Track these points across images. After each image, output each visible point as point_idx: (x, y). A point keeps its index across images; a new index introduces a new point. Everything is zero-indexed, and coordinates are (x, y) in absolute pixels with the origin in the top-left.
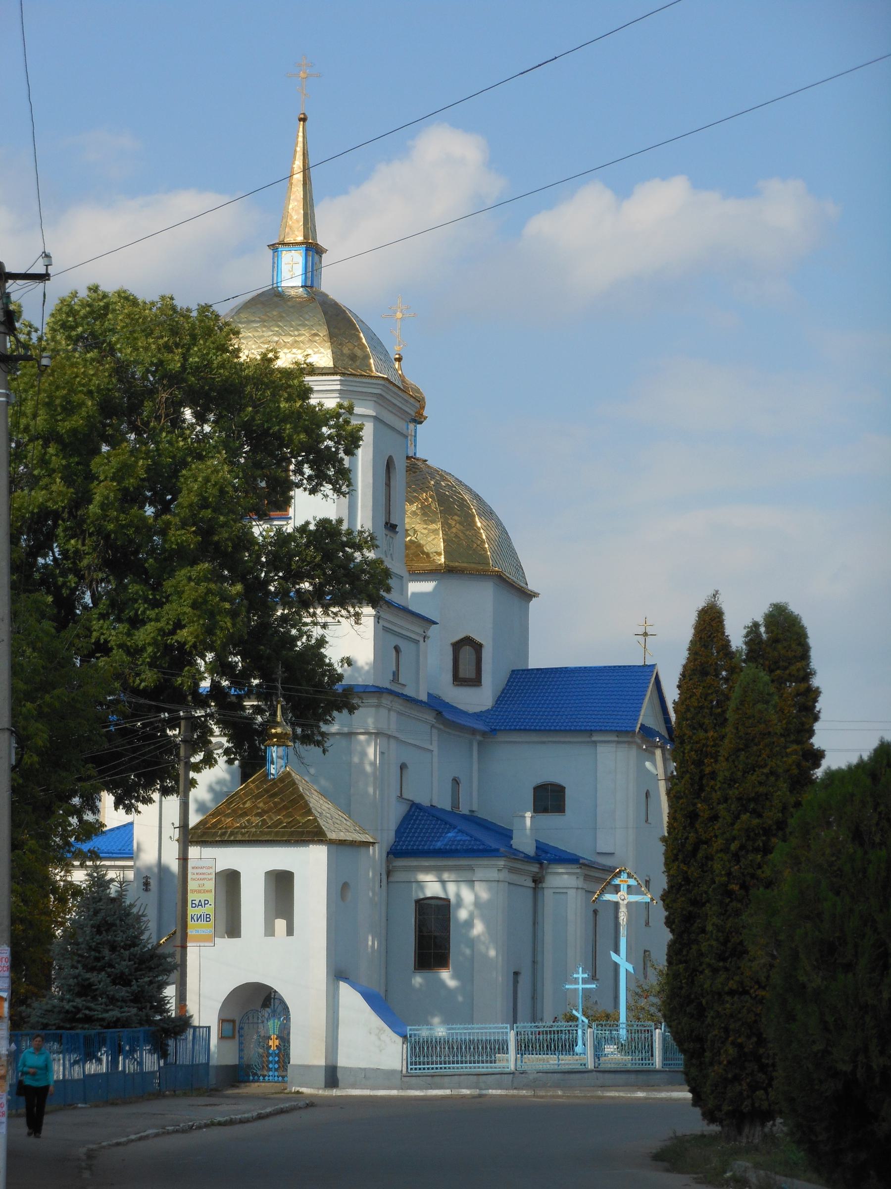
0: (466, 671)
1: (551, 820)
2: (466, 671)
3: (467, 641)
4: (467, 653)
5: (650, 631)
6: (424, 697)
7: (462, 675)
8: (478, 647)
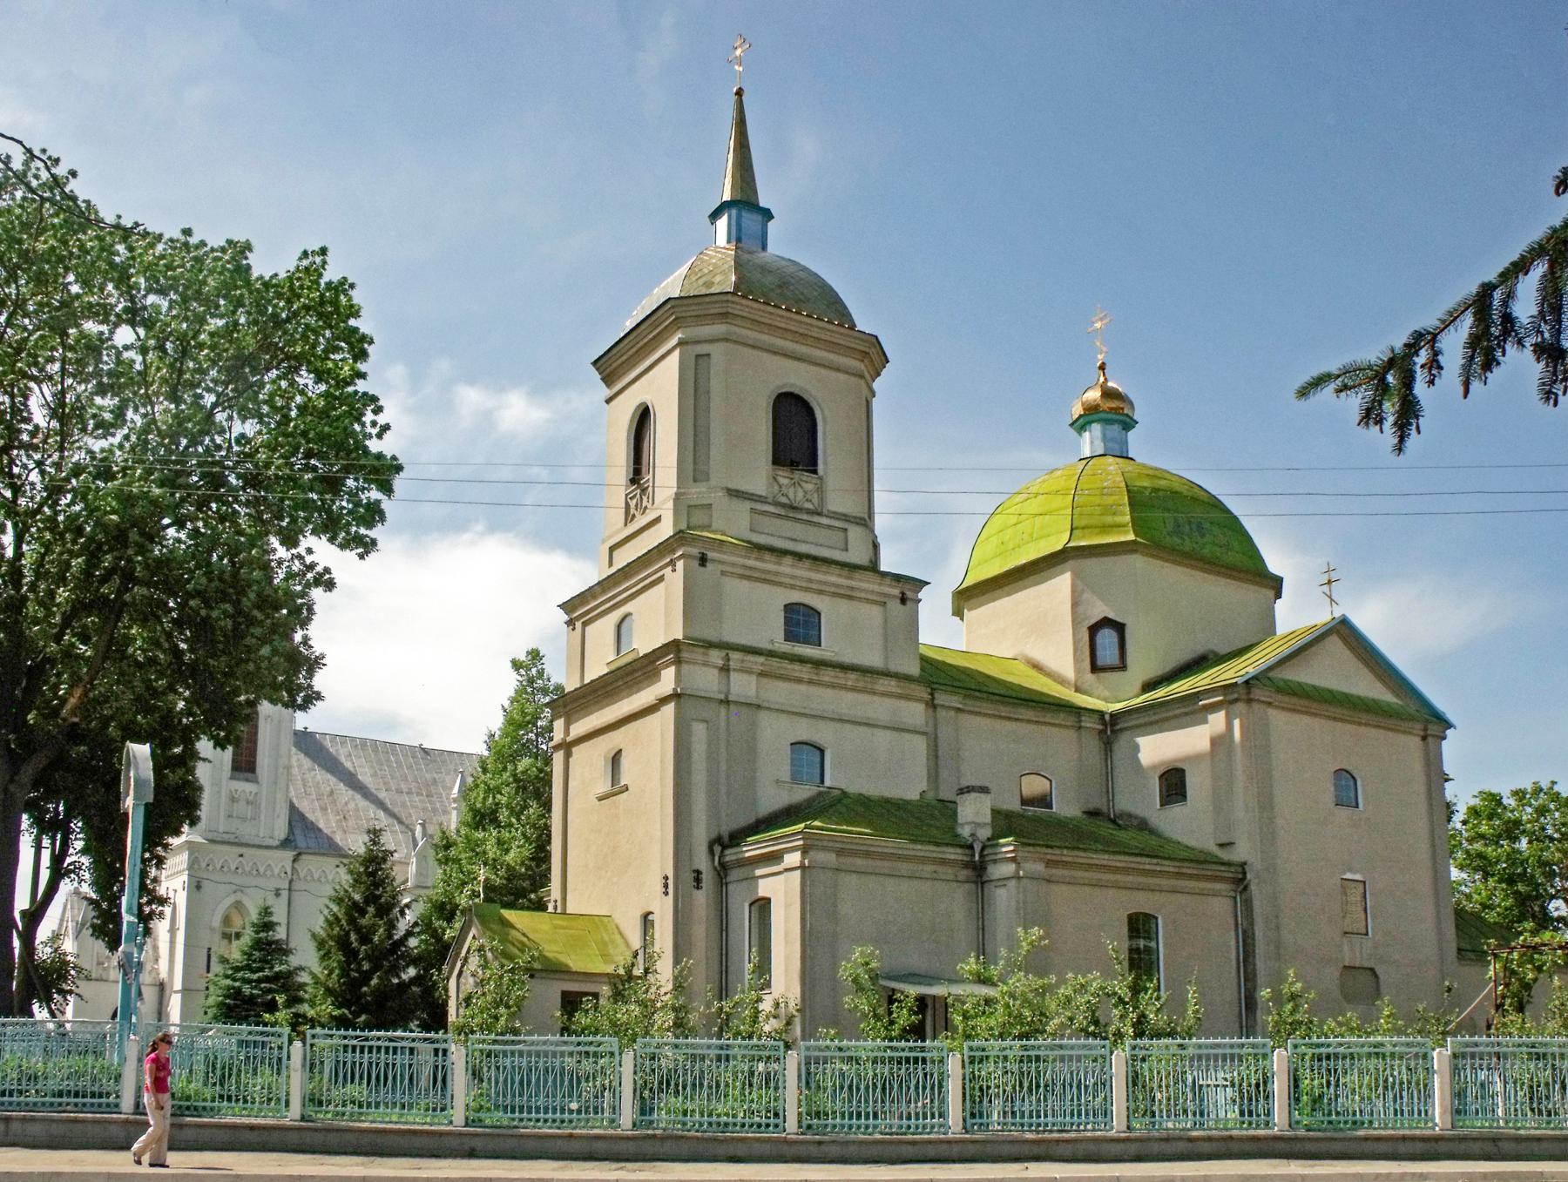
0: (1108, 654)
1: (1176, 810)
2: (1108, 654)
3: (1106, 622)
4: (1107, 638)
5: (1334, 576)
6: (914, 669)
7: (1100, 663)
8: (1120, 628)
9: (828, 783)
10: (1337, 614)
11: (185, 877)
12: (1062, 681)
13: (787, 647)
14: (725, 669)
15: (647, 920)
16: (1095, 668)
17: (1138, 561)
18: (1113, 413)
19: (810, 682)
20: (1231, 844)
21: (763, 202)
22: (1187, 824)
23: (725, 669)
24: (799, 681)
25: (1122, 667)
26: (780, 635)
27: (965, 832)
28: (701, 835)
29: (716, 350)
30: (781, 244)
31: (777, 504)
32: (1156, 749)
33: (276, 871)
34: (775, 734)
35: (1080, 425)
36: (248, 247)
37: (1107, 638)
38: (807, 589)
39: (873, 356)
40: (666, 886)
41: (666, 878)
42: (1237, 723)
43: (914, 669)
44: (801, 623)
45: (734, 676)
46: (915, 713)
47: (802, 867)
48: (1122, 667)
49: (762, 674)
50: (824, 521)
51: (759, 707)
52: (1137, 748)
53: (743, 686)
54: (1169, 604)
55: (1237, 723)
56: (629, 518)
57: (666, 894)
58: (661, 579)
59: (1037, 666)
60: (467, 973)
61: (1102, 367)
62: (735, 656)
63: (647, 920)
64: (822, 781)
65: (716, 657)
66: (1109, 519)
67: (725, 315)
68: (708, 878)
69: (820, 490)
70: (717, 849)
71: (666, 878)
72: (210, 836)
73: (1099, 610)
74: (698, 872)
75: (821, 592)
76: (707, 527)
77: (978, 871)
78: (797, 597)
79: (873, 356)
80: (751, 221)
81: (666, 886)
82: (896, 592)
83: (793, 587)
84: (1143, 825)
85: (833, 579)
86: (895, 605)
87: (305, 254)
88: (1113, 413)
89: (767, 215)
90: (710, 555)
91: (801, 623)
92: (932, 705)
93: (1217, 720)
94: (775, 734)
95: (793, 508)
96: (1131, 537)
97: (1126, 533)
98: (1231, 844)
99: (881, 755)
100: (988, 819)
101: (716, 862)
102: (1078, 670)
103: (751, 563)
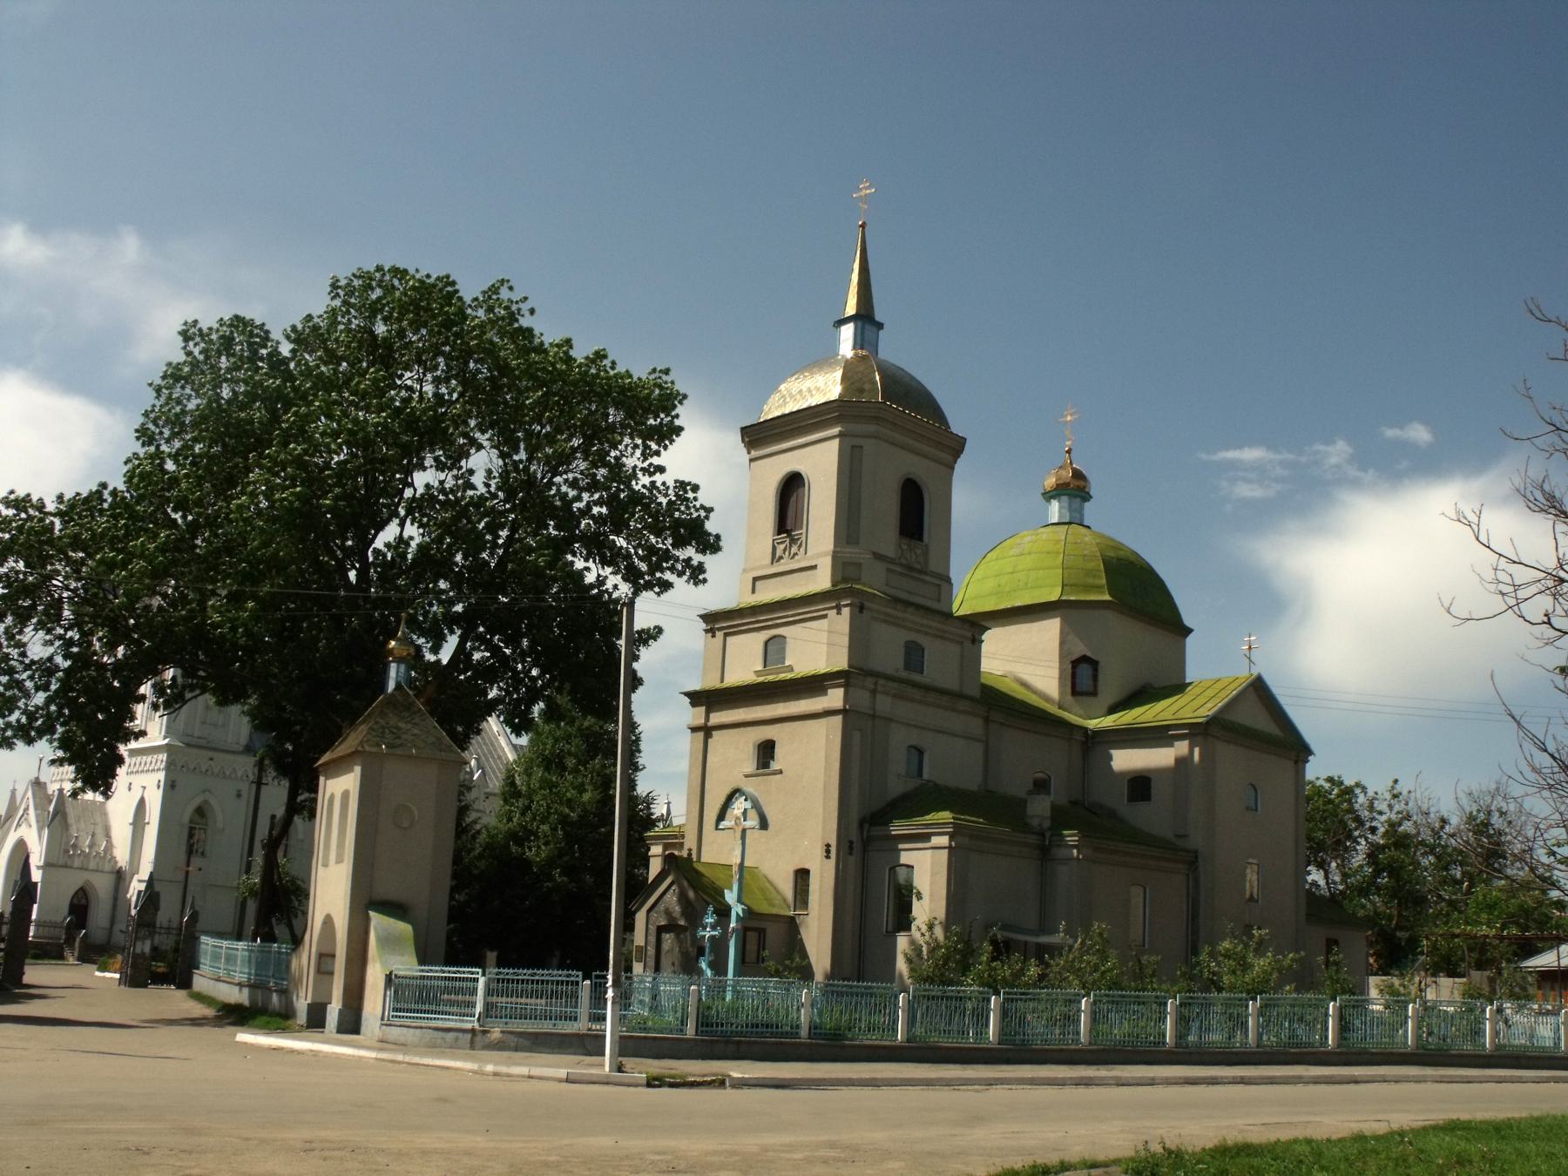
3: (1084, 659)
6: (976, 693)
8: (1094, 664)
9: (926, 776)
10: (1255, 674)
11: (161, 776)
12: (1047, 699)
13: (904, 674)
14: (874, 692)
15: (802, 875)
16: (1075, 693)
17: (1110, 615)
18: (1075, 489)
19: (920, 702)
20: (1185, 836)
21: (878, 318)
22: (1151, 817)
23: (874, 692)
24: (912, 700)
25: (1094, 693)
26: (900, 664)
27: (1035, 822)
28: (854, 816)
29: (869, 445)
30: (891, 349)
31: (901, 565)
32: (1125, 760)
33: (239, 774)
34: (900, 739)
35: (1049, 496)
36: (568, 342)
37: (1085, 670)
38: (918, 631)
39: (956, 446)
40: (828, 851)
41: (828, 846)
42: (1197, 750)
43: (976, 693)
44: (914, 655)
45: (879, 698)
46: (975, 725)
47: (950, 848)
48: (1094, 693)
49: (895, 696)
50: (928, 578)
51: (890, 720)
52: (1110, 758)
53: (884, 704)
54: (1124, 648)
55: (1197, 750)
56: (775, 559)
57: (828, 857)
58: (825, 616)
59: (1025, 685)
60: (661, 907)
61: (1069, 452)
62: (882, 682)
63: (802, 875)
64: (920, 774)
65: (869, 682)
66: (1090, 581)
67: (876, 418)
68: (857, 846)
69: (926, 553)
70: (866, 826)
71: (828, 846)
72: (187, 740)
73: (1080, 649)
74: (851, 842)
75: (927, 634)
76: (858, 581)
77: (1045, 851)
78: (913, 636)
79: (956, 446)
80: (869, 329)
81: (828, 851)
82: (969, 635)
83: (910, 629)
84: (1112, 814)
85: (935, 624)
86: (968, 644)
87: (654, 370)
88: (1075, 489)
89: (880, 326)
90: (867, 604)
91: (914, 655)
92: (987, 720)
93: (1182, 747)
94: (900, 739)
95: (910, 568)
96: (1107, 597)
97: (1102, 593)
98: (1185, 836)
99: (954, 758)
100: (1048, 814)
101: (867, 833)
102: (1061, 693)
103: (889, 611)
